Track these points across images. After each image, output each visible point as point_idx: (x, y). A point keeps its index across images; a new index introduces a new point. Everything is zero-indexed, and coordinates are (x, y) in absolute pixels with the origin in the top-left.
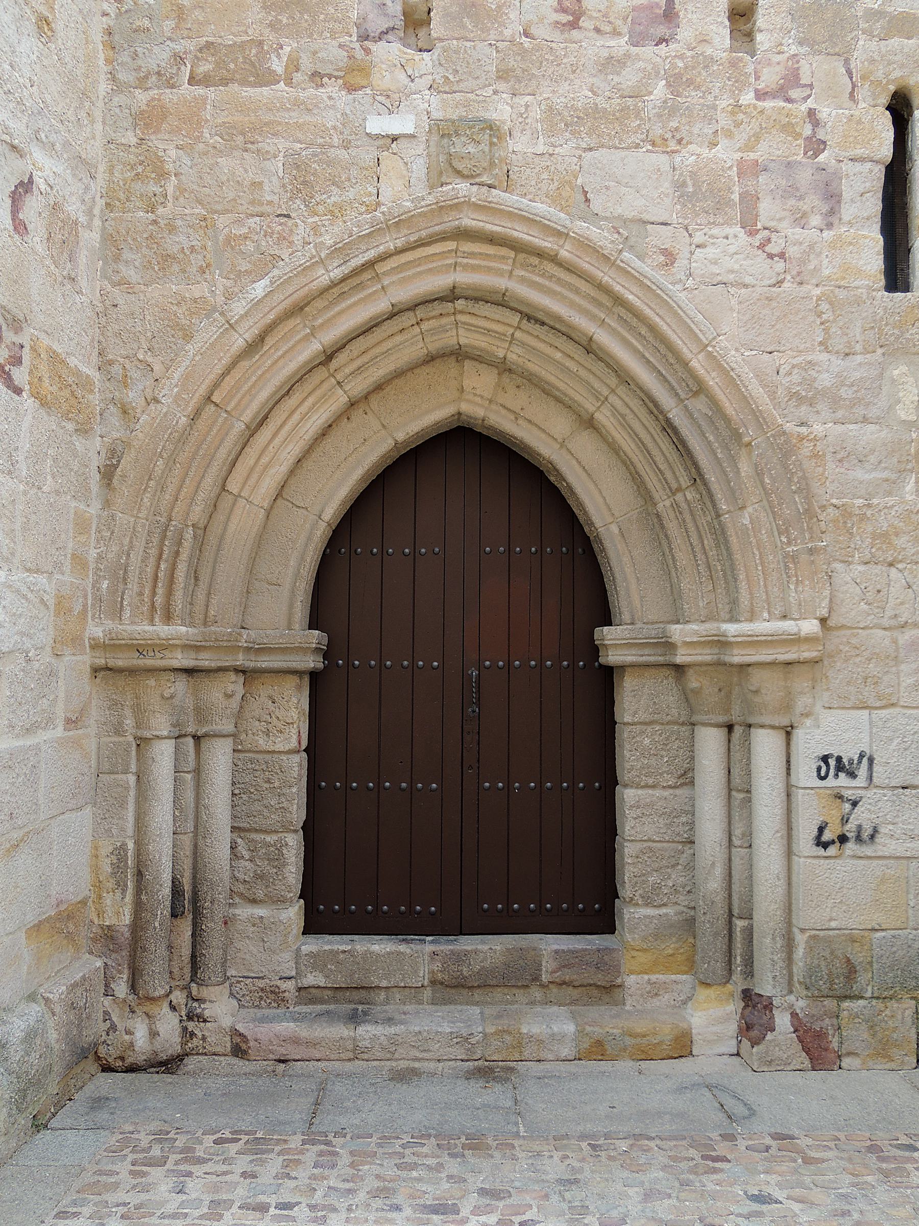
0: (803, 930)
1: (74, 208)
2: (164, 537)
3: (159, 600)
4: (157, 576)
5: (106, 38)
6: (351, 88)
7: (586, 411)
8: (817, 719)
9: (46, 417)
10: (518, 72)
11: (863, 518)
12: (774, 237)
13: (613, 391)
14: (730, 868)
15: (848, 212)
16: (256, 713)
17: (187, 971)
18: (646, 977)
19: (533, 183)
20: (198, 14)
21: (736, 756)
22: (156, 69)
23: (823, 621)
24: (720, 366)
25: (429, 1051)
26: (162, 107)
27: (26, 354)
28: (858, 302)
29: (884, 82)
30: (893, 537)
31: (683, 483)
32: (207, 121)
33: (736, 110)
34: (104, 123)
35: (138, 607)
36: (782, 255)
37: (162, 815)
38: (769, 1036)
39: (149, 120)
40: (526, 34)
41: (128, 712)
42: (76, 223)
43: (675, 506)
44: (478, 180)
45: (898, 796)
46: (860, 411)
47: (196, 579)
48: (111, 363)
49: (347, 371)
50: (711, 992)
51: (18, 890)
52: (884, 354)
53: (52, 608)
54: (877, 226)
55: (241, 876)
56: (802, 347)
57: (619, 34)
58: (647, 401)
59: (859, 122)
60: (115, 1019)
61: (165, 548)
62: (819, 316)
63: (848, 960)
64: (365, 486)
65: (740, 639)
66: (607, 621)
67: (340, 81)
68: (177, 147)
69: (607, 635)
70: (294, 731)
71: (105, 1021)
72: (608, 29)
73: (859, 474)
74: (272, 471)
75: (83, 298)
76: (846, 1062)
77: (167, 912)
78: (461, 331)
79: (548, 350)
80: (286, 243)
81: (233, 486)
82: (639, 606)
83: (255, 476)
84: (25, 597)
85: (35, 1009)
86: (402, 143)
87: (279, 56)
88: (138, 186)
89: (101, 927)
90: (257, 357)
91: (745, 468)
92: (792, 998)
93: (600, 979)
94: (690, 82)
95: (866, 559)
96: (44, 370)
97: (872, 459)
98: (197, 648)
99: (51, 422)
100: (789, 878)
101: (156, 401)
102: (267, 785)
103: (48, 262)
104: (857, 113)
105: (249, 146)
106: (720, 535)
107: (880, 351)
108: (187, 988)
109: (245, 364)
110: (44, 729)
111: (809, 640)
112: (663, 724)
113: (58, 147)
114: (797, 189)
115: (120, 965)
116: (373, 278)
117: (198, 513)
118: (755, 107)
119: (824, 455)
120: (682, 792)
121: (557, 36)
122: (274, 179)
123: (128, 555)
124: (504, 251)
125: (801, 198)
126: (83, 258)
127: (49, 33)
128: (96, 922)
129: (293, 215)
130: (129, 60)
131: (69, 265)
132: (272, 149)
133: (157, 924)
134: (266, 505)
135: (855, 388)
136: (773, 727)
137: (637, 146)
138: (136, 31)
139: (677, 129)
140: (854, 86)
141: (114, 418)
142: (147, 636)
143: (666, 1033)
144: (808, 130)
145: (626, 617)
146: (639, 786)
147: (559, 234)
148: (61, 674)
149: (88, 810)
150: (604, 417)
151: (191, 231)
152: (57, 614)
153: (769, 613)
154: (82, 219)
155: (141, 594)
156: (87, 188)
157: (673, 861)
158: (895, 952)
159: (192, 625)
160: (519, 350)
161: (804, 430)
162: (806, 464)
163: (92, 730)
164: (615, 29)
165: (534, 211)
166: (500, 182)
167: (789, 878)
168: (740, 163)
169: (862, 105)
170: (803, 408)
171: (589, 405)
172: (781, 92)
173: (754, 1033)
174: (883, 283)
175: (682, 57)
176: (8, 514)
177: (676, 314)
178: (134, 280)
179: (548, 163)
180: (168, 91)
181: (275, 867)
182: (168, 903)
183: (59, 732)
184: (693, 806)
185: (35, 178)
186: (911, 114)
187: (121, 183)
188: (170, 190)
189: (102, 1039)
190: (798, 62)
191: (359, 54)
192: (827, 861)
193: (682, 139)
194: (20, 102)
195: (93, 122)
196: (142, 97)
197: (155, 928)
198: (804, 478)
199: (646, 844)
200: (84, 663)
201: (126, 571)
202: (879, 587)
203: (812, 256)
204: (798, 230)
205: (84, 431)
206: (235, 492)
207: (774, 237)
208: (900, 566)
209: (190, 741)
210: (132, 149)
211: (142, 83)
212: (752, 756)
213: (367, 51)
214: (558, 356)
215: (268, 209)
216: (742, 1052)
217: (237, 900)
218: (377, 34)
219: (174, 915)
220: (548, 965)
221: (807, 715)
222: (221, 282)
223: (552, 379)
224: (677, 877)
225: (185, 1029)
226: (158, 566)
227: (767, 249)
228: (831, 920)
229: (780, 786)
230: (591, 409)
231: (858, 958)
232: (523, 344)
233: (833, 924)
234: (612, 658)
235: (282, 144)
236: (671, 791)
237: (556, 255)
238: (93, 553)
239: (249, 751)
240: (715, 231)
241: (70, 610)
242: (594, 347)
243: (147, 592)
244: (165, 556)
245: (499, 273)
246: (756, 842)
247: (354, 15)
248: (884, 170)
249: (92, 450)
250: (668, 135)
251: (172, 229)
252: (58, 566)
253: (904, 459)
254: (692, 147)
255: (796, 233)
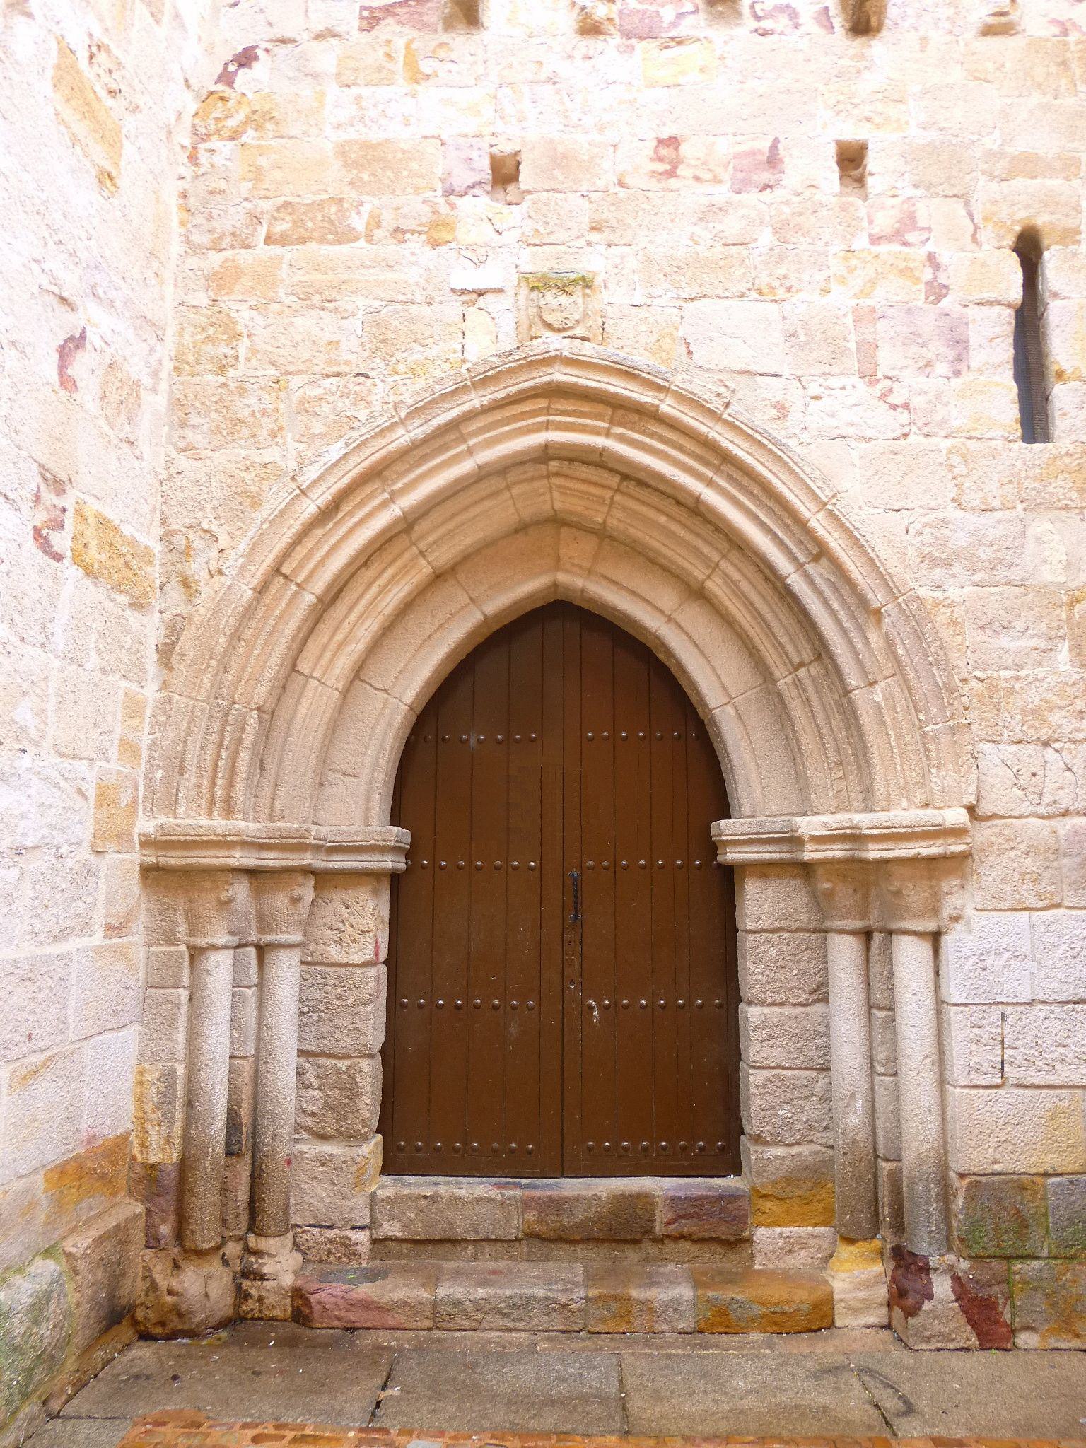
0: (962, 1176)
1: (137, 369)
2: (225, 722)
3: (219, 791)
4: (216, 765)
5: (181, 201)
6: (435, 244)
7: (696, 579)
8: (968, 923)
9: (92, 587)
10: (613, 223)
11: (1011, 692)
12: (896, 386)
13: (724, 556)
14: (873, 1100)
15: (977, 358)
16: (328, 921)
17: (244, 1218)
18: (778, 1230)
19: (631, 335)
20: (278, 175)
21: (876, 968)
22: (232, 230)
23: (971, 809)
24: (843, 526)
25: (522, 1320)
26: (236, 267)
27: (69, 520)
28: (994, 454)
29: (1009, 223)
30: (1046, 713)
31: (805, 656)
32: (282, 280)
33: (850, 254)
34: (175, 285)
35: (195, 800)
36: (906, 406)
37: (218, 1039)
38: (927, 1306)
39: (220, 281)
40: (621, 184)
41: (180, 918)
42: (137, 384)
43: (798, 683)
44: (570, 333)
45: (1068, 1013)
46: (1002, 573)
47: (262, 769)
48: (173, 533)
49: (430, 539)
50: (861, 1248)
51: (36, 1124)
52: (1025, 510)
53: (92, 798)
54: (1010, 374)
55: (309, 1108)
56: (933, 504)
57: (720, 182)
58: (762, 566)
59: (984, 265)
60: (156, 1276)
61: (227, 734)
62: (950, 470)
63: (1018, 1213)
64: (452, 666)
65: (875, 832)
66: (725, 811)
67: (424, 237)
68: (251, 308)
69: (725, 828)
70: (369, 939)
71: (144, 1278)
72: (708, 176)
73: (1004, 641)
74: (349, 649)
75: (144, 464)
76: (1023, 1339)
77: (220, 1149)
78: (556, 495)
79: (652, 514)
80: (363, 404)
81: (304, 667)
82: (760, 797)
83: (328, 655)
84: (56, 785)
85: (47, 1268)
86: (489, 297)
87: (359, 213)
88: (208, 349)
89: (144, 1165)
90: (331, 525)
91: (874, 638)
92: (951, 1258)
93: (723, 1231)
94: (798, 229)
95: (1015, 738)
96: (91, 536)
97: (1019, 625)
98: (262, 847)
99: (95, 593)
100: (943, 1112)
101: (220, 572)
102: (339, 1003)
103: (102, 422)
104: (980, 255)
105: (327, 304)
106: (849, 714)
107: (1020, 507)
108: (242, 1239)
109: (319, 532)
110: (79, 935)
111: (957, 832)
112: (791, 932)
113: (118, 304)
114: (919, 336)
115: (163, 1211)
116: (457, 439)
117: (261, 694)
118: (869, 252)
119: (963, 622)
120: (818, 1008)
121: (654, 185)
122: (353, 338)
123: (186, 742)
124: (600, 408)
125: (923, 345)
126: (145, 421)
127: (112, 189)
128: (139, 1159)
129: (371, 374)
130: (204, 222)
131: (127, 428)
132: (350, 307)
133: (207, 1164)
134: (340, 687)
135: (994, 548)
136: (916, 933)
137: (743, 295)
138: (211, 193)
139: (785, 277)
140: (976, 228)
141: (175, 593)
142: (202, 831)
143: (802, 1297)
144: (928, 274)
145: (746, 809)
146: (763, 1004)
147: (659, 388)
148: (102, 874)
149: (135, 1029)
150: (715, 586)
151: (263, 393)
152: (98, 806)
153: (908, 800)
154: (147, 381)
155: (198, 786)
156: (152, 350)
157: (807, 1093)
158: (1074, 1202)
159: (257, 820)
160: (619, 514)
161: (938, 594)
162: (944, 633)
163: (140, 939)
164: (715, 177)
165: (632, 364)
166: (595, 335)
167: (943, 1112)
168: (856, 310)
169: (986, 247)
170: (937, 570)
171: (698, 572)
172: (897, 236)
173: (910, 1301)
174: (1019, 433)
175: (787, 203)
176: (38, 691)
177: (791, 471)
178: (200, 446)
179: (647, 315)
180: (243, 251)
181: (347, 1098)
182: (222, 1140)
183: (98, 939)
184: (828, 1026)
185: (89, 334)
186: (1040, 255)
187: (191, 346)
188: (242, 352)
189: (140, 1301)
190: (914, 205)
191: (444, 209)
192: (988, 1091)
193: (791, 287)
194: (73, 254)
195: (162, 283)
196: (215, 259)
197: (205, 1168)
198: (942, 647)
199: (774, 1072)
200: (133, 862)
201: (182, 760)
202: (1033, 770)
203: (939, 406)
204: (922, 379)
205: (139, 605)
206: (306, 672)
207: (896, 386)
208: (1057, 745)
209: (252, 951)
210: (205, 311)
211: (216, 247)
212: (895, 968)
213: (452, 206)
214: (663, 519)
215: (343, 368)
216: (894, 1323)
217: (304, 1135)
218: (463, 189)
219: (229, 1153)
220: (661, 1216)
221: (956, 919)
222: (293, 446)
223: (657, 545)
224: (812, 1111)
225: (239, 1287)
226: (219, 755)
227: (889, 399)
228: (995, 1162)
229: (929, 1002)
230: (701, 577)
231: (1031, 1209)
232: (624, 508)
233: (998, 1168)
234: (732, 856)
235: (361, 302)
236: (802, 1009)
237: (657, 410)
238: (146, 740)
239: (320, 964)
240: (833, 382)
241: (115, 802)
242: (702, 508)
243: (206, 783)
244: (226, 743)
245: (595, 431)
246: (903, 1069)
247: (439, 172)
248: (1013, 313)
249: (150, 628)
250: (776, 283)
251: (242, 391)
252: (102, 752)
253: (1054, 624)
254: (800, 295)
255: (921, 381)
